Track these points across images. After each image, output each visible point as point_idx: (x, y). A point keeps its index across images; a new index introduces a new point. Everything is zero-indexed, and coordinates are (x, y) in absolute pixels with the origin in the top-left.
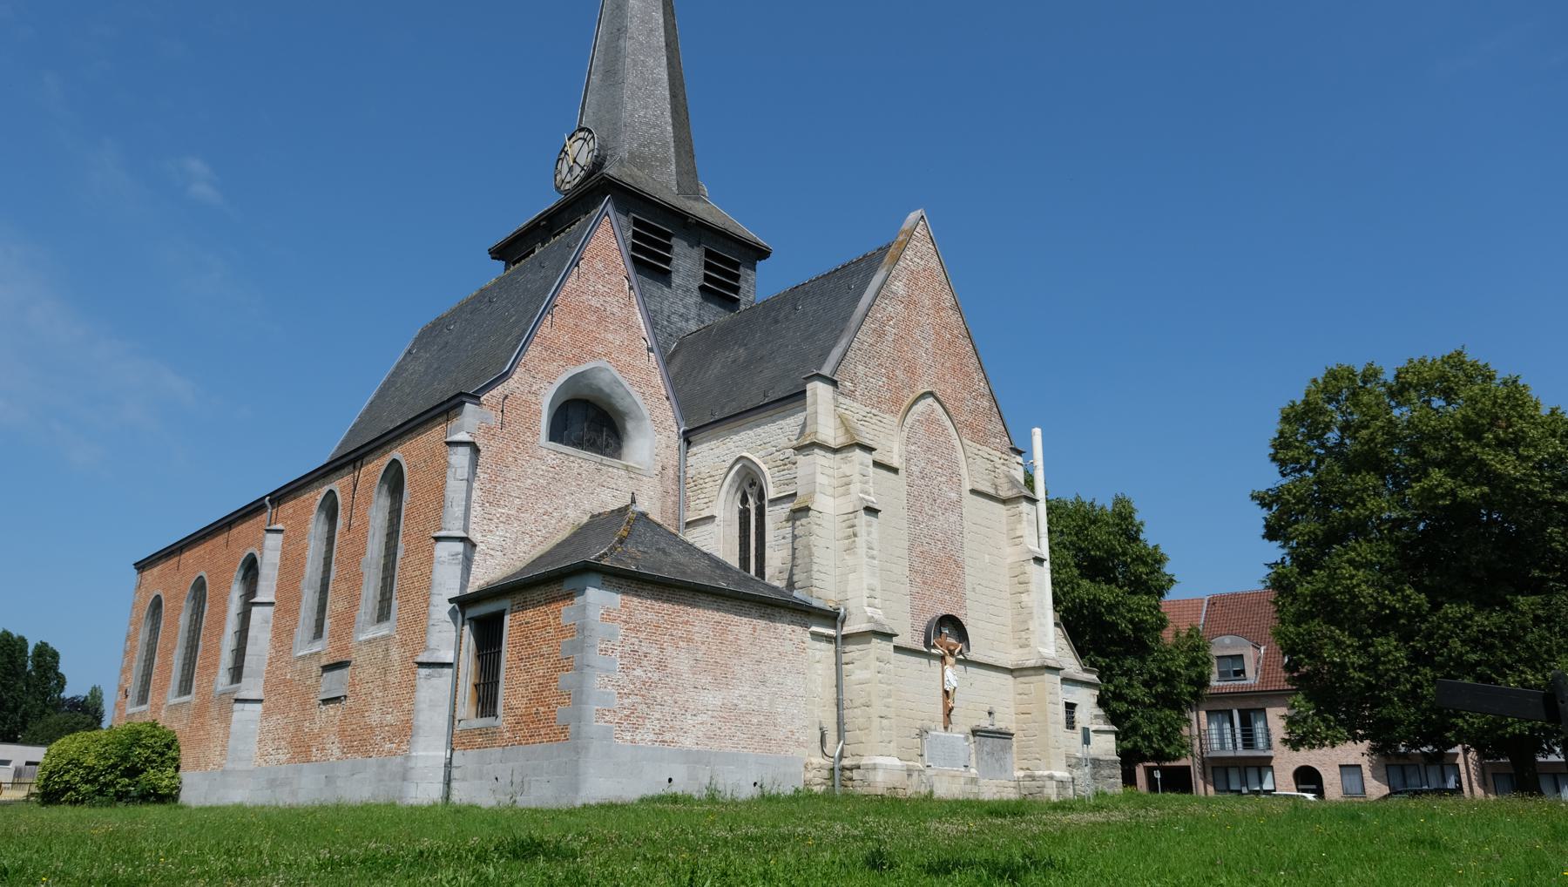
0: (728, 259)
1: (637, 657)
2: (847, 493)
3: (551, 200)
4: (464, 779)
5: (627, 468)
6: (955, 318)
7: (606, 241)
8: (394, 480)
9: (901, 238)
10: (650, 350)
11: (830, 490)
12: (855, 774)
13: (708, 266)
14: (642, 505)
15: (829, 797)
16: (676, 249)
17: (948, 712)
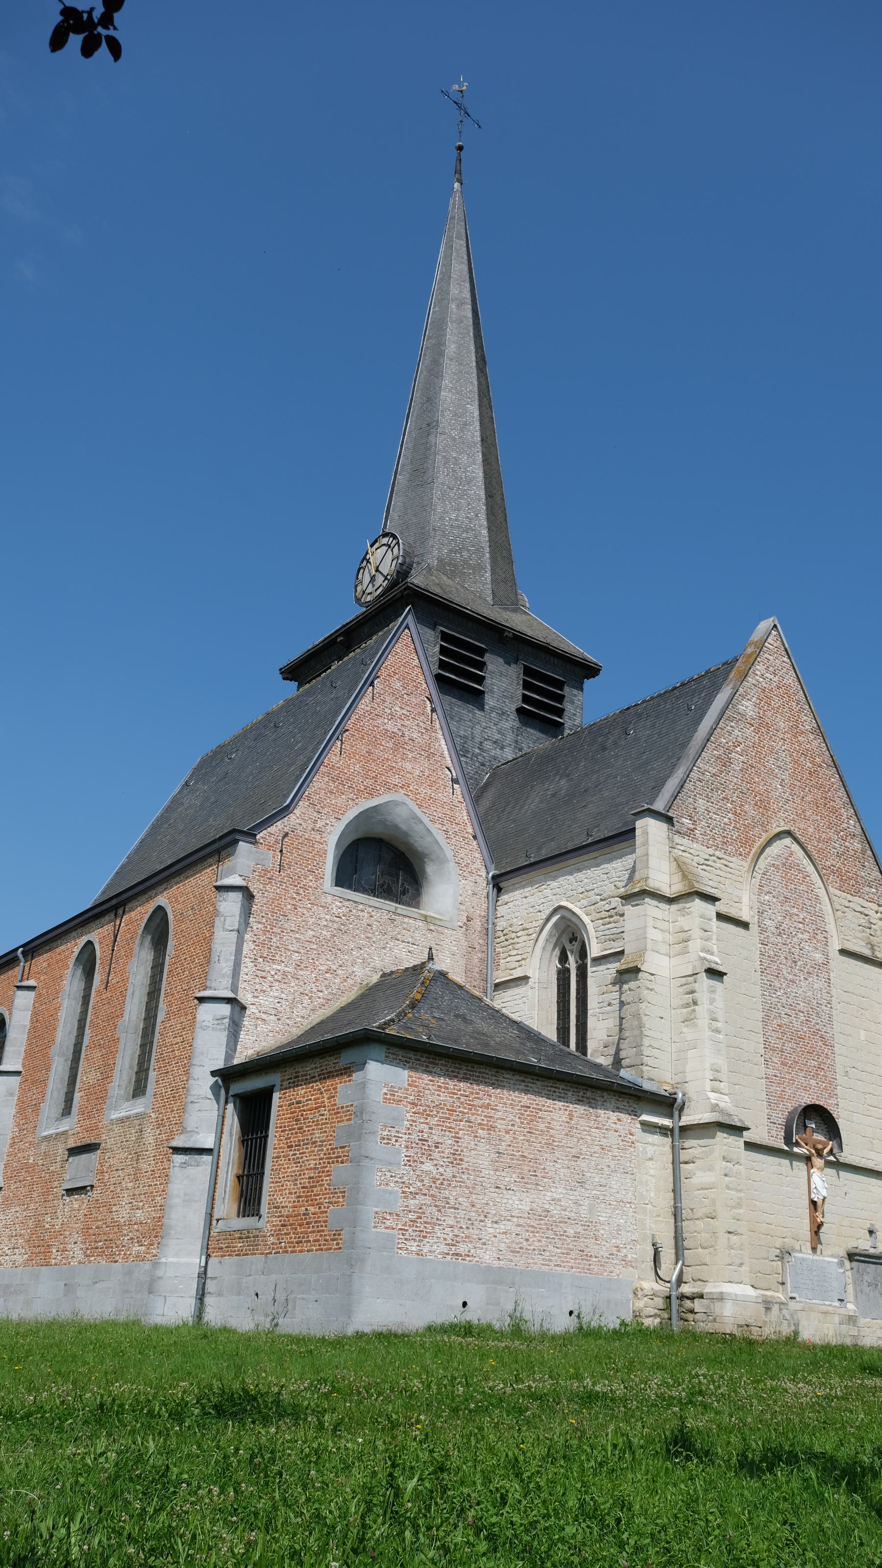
0: (551, 677)
1: (425, 1147)
2: (685, 952)
3: (352, 612)
4: (220, 1295)
5: (425, 919)
6: (816, 743)
7: (407, 658)
8: (158, 930)
9: (749, 650)
10: (455, 781)
11: (664, 948)
12: (697, 1305)
13: (527, 685)
14: (442, 963)
15: (664, 1335)
16: (490, 667)
17: (816, 1229)
